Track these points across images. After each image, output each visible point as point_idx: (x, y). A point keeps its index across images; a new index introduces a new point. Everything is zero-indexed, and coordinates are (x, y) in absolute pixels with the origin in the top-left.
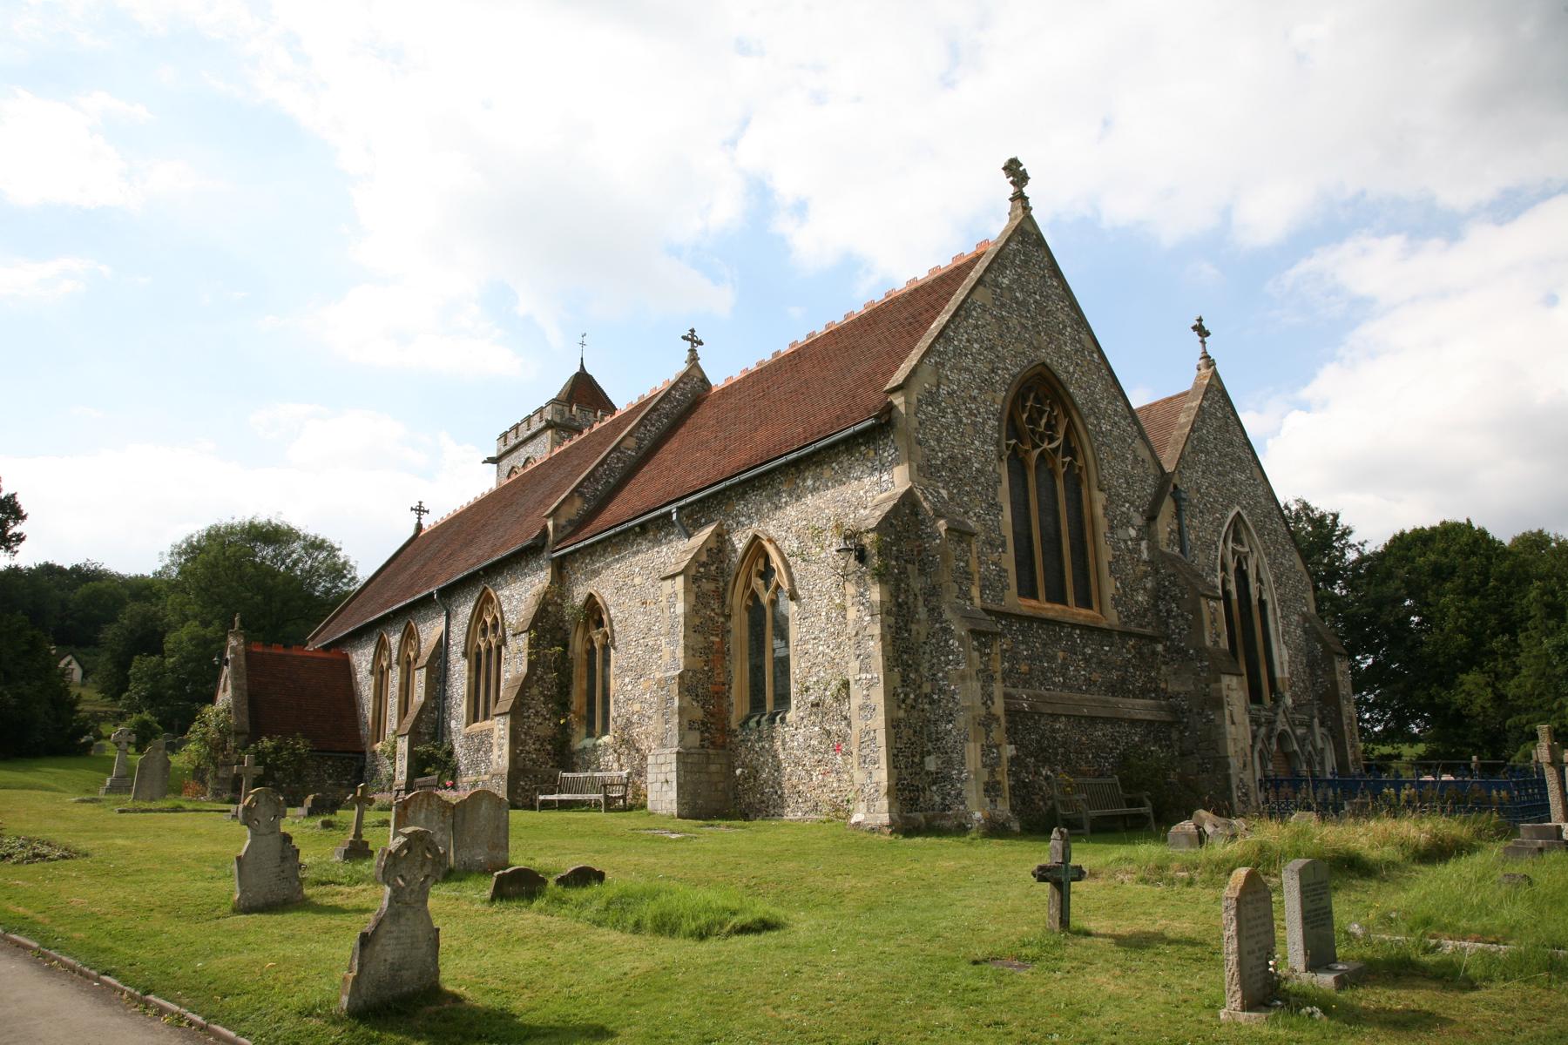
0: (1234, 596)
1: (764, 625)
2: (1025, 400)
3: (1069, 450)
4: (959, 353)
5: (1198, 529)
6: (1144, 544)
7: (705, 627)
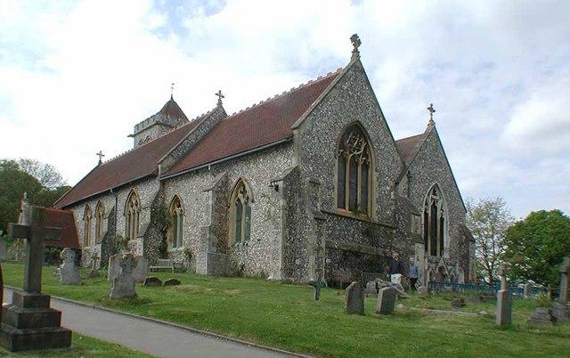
0: (430, 215)
1: (243, 210)
2: (349, 134)
3: (365, 154)
4: (322, 115)
5: (416, 188)
6: (392, 193)
7: (220, 208)
